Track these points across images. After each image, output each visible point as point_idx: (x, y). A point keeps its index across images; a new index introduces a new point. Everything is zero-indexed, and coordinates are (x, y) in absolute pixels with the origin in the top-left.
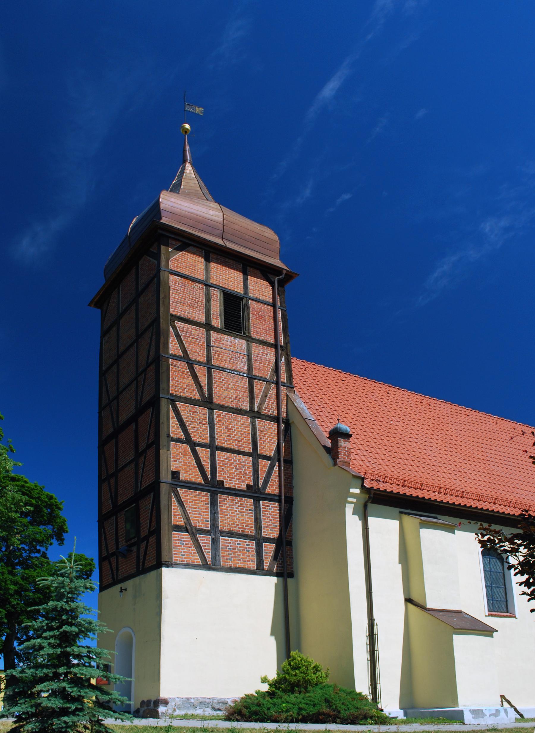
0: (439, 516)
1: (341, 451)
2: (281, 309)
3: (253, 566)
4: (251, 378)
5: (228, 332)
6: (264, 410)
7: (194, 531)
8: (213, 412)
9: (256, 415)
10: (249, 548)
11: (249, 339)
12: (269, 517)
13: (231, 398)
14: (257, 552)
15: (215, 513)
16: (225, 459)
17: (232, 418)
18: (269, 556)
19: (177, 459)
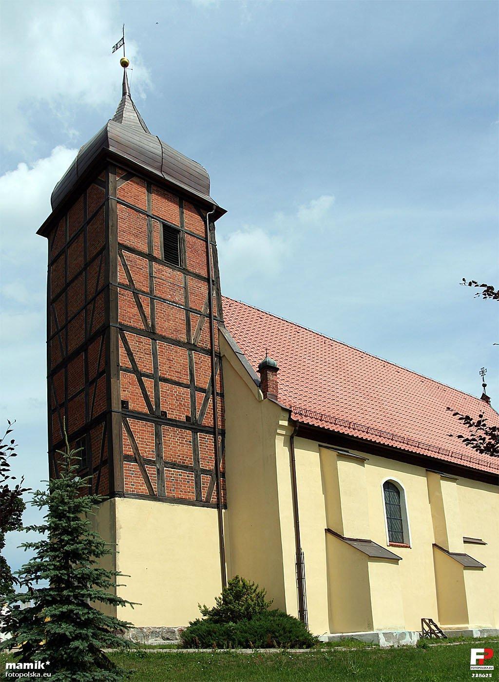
0: (350, 451)
1: (270, 384)
2: (212, 244)
3: (192, 496)
4: (188, 310)
5: (168, 264)
6: (199, 343)
7: (142, 461)
8: (156, 342)
9: (193, 347)
10: (189, 479)
11: (186, 272)
12: (205, 449)
13: (171, 330)
14: (196, 483)
15: (160, 444)
16: (167, 390)
17: (173, 349)
18: (206, 487)
19: (126, 388)
